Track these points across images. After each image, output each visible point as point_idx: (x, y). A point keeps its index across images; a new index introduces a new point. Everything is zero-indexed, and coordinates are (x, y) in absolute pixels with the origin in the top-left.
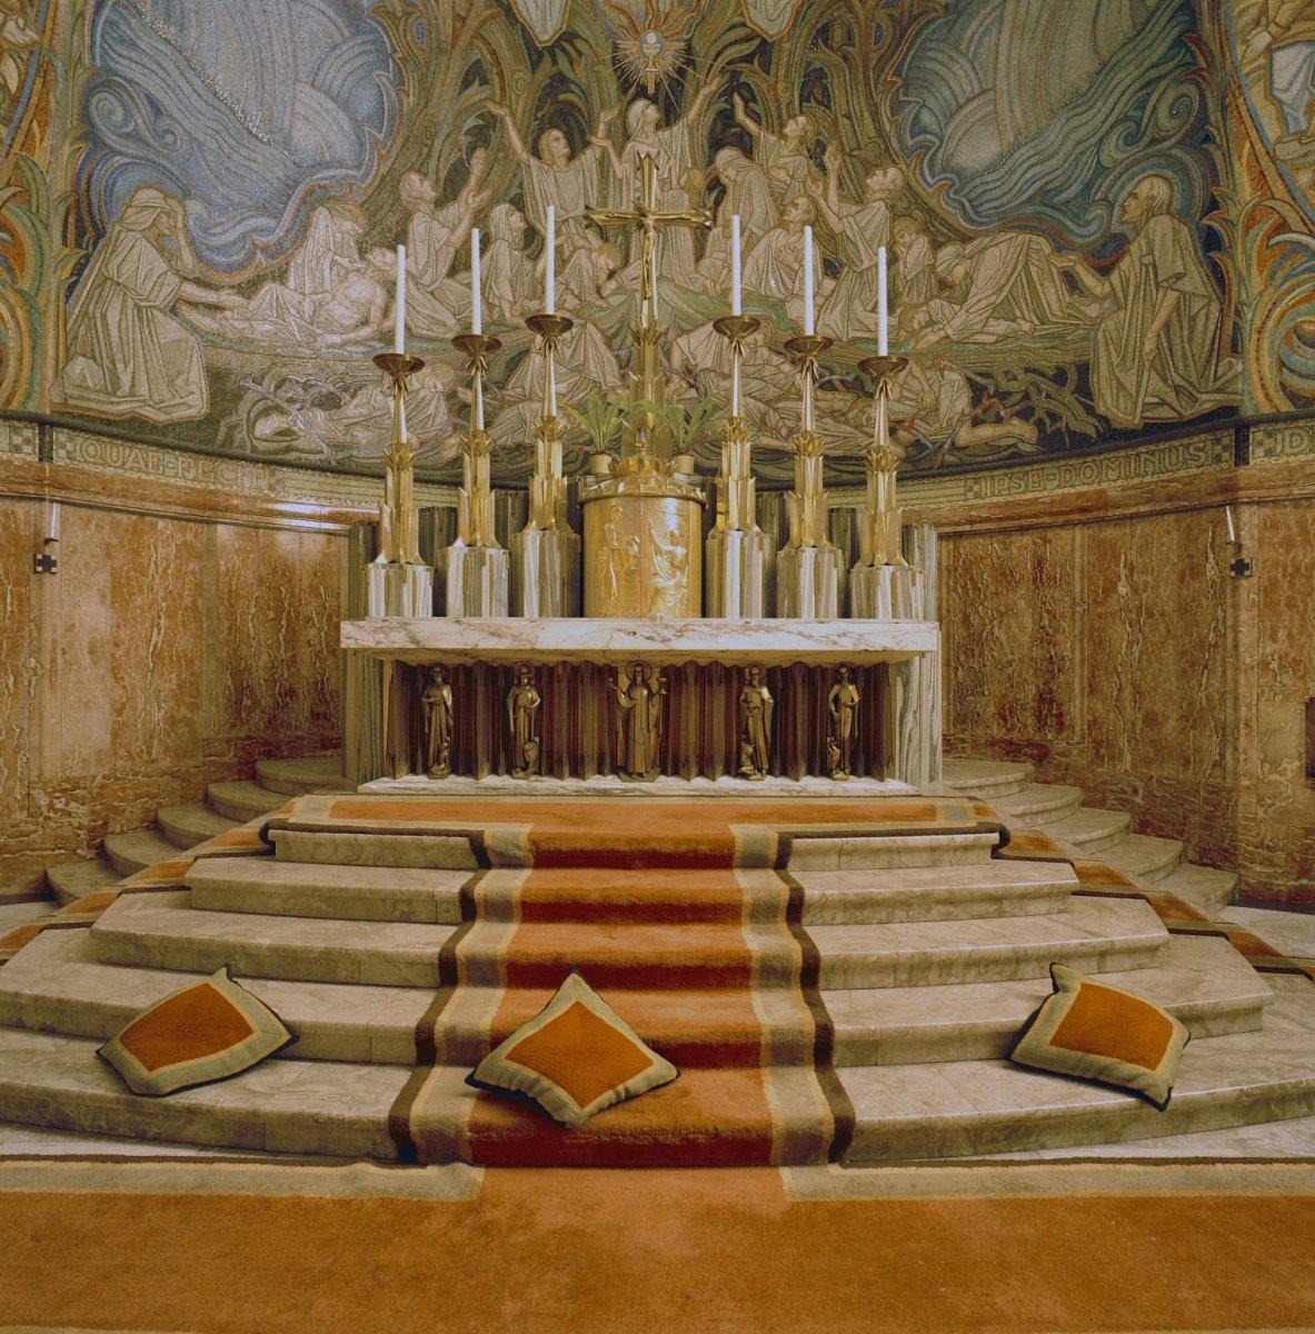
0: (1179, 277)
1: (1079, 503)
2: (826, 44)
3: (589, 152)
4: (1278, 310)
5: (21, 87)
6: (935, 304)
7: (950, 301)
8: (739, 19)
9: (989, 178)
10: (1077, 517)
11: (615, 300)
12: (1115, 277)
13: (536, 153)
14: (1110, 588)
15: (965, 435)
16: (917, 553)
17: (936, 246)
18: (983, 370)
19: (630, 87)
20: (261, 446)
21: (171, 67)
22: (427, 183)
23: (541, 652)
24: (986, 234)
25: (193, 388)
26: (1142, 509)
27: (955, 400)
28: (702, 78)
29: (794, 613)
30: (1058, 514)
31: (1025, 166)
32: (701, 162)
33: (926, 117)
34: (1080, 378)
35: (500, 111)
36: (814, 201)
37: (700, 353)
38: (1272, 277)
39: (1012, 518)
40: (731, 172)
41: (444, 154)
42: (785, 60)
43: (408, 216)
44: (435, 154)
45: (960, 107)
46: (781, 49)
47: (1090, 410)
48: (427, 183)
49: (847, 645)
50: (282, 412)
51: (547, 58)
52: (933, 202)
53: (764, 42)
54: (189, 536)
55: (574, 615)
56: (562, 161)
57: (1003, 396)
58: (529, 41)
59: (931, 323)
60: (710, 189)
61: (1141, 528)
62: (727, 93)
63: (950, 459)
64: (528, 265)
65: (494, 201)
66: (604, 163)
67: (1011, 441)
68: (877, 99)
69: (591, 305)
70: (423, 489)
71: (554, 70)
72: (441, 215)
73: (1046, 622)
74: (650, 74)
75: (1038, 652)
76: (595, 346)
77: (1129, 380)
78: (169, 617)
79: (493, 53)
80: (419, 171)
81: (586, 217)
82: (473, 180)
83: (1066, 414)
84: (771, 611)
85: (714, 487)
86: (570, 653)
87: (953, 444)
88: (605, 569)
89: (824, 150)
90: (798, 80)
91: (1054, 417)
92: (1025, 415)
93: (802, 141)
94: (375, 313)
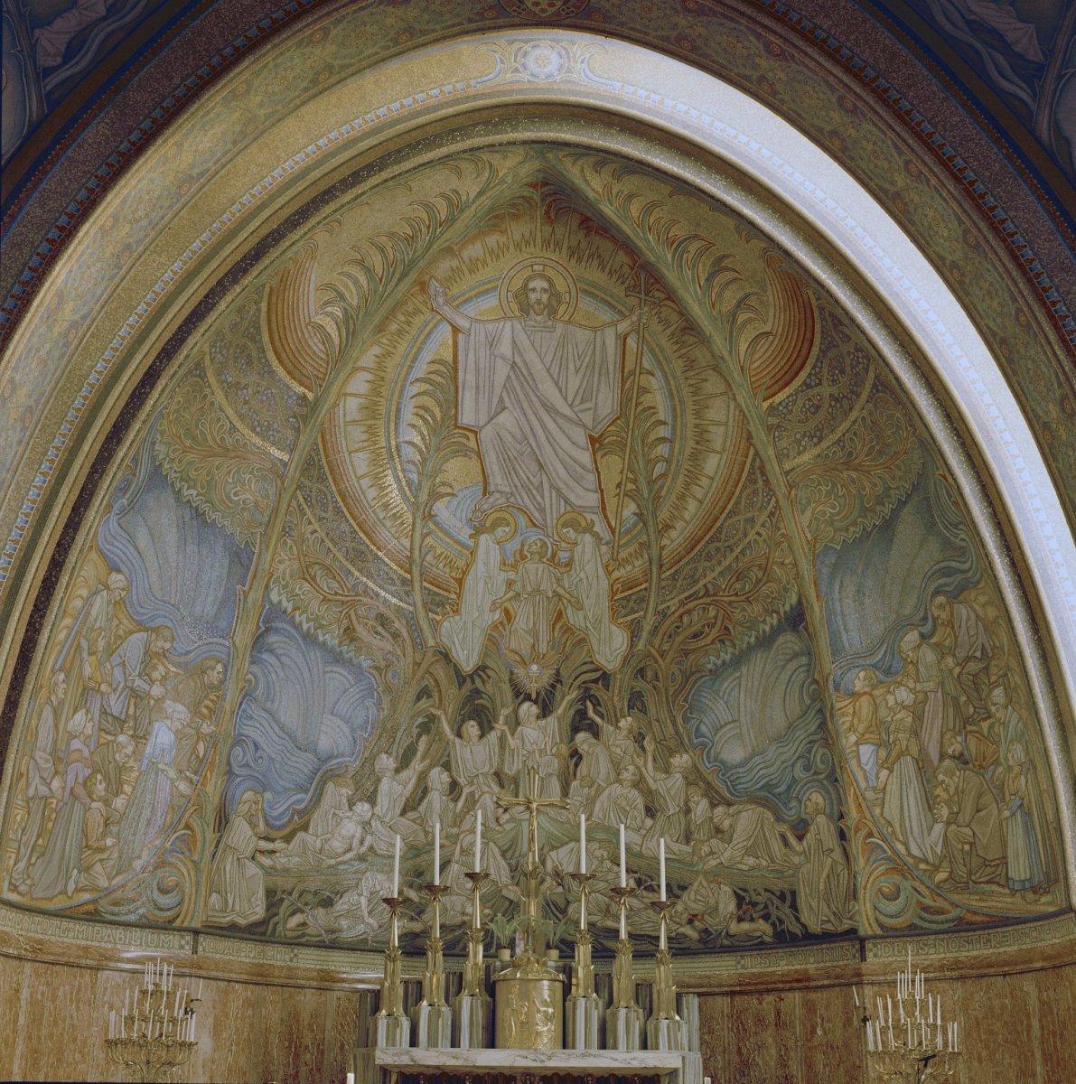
0: (832, 851)
1: (796, 976)
2: (642, 678)
3: (493, 733)
4: (872, 879)
5: (204, 755)
6: (714, 841)
7: (721, 839)
8: (589, 659)
9: (740, 770)
10: (795, 985)
11: (508, 827)
12: (805, 842)
13: (459, 735)
14: (813, 1032)
15: (734, 928)
16: (685, 1011)
17: (713, 806)
18: (743, 887)
19: (520, 694)
20: (289, 934)
21: (266, 724)
22: (391, 759)
23: (478, 1067)
24: (740, 803)
25: (259, 902)
26: (826, 982)
27: (728, 906)
28: (566, 690)
29: (615, 1047)
30: (787, 982)
31: (758, 768)
32: (566, 741)
33: (703, 729)
34: (789, 898)
35: (438, 713)
36: (638, 768)
37: (565, 862)
38: (868, 859)
39: (762, 983)
40: (585, 747)
41: (403, 741)
42: (618, 684)
43: (379, 780)
44: (397, 741)
45: (722, 727)
46: (615, 678)
47: (798, 919)
48: (391, 759)
49: (636, 1064)
50: (303, 912)
51: (468, 680)
52: (710, 778)
53: (604, 673)
54: (249, 993)
55: (488, 1047)
56: (475, 739)
57: (754, 904)
58: (457, 671)
59: (712, 853)
60: (572, 756)
61: (826, 994)
62: (582, 700)
63: (726, 942)
64: (451, 805)
65: (431, 766)
66: (502, 741)
67: (758, 934)
68: (674, 713)
69: (493, 830)
70: (499, 1040)
71: (472, 687)
72: (398, 777)
73: (783, 1052)
74: (532, 688)
75: (780, 1073)
76: (495, 858)
77: (814, 904)
78: (237, 1045)
79: (436, 680)
80: (386, 753)
81: (497, 803)
82: (419, 755)
83: (786, 921)
84: (603, 1045)
85: (570, 968)
86: (493, 1068)
87: (727, 933)
88: (509, 1022)
89: (644, 739)
90: (627, 697)
91: (781, 921)
92: (766, 917)
93: (630, 731)
94: (356, 843)
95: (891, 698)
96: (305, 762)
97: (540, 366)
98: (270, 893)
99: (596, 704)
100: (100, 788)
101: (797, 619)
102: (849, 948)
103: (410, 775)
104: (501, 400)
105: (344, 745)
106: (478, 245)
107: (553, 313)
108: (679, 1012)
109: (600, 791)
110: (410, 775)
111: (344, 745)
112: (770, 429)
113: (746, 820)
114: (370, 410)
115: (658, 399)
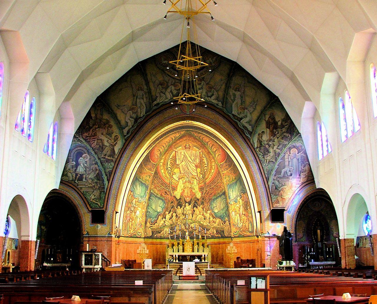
15: (216, 235)
17: (213, 218)
27: (215, 232)
34: (223, 231)
35: (174, 205)
41: (169, 211)
57: (218, 232)
62: (195, 203)
66: (183, 208)
92: (220, 234)
94: (163, 224)
95: (236, 206)
96: (156, 213)
97: (188, 156)
98: (152, 232)
99: (197, 203)
100: (131, 220)
101: (224, 193)
102: (231, 239)
103: (171, 214)
104: (182, 160)
105: (161, 211)
106: (179, 141)
107: (189, 149)
108: (208, 247)
109: (197, 216)
110: (171, 214)
111: (161, 211)
112: (220, 167)
113: (218, 220)
114: (164, 164)
115: (205, 161)
